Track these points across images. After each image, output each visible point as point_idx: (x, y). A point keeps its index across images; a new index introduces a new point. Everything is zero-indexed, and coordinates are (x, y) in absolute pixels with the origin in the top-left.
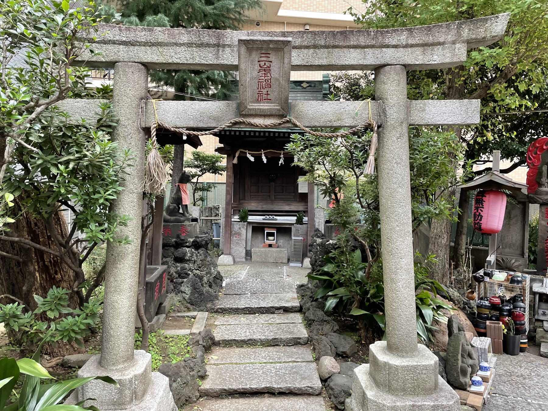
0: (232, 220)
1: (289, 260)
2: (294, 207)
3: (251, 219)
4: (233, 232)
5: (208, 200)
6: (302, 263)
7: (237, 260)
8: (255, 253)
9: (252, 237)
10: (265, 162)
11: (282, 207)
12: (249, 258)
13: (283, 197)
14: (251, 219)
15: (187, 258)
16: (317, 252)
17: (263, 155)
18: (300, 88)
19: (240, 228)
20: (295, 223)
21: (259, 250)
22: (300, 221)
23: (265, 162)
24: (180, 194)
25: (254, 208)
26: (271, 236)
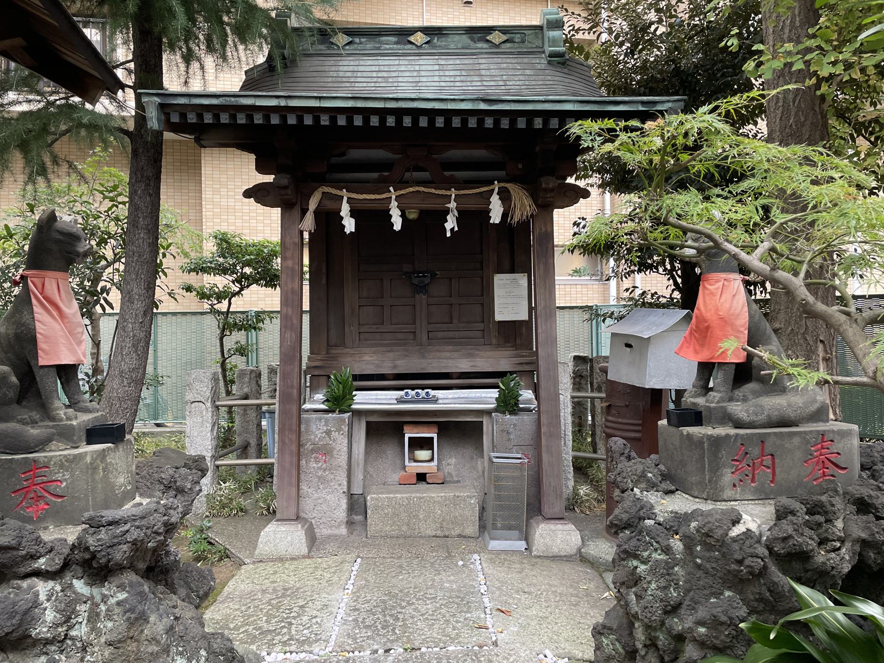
0: (307, 406)
1: (482, 528)
2: (485, 361)
3: (364, 400)
4: (309, 446)
5: (261, 353)
6: (527, 538)
7: (322, 531)
8: (376, 508)
9: (367, 453)
10: (397, 227)
12: (359, 518)
13: (451, 334)
15: (41, 631)
16: (669, 567)
17: (394, 204)
18: (485, 45)
19: (328, 433)
20: (496, 410)
21: (388, 498)
22: (509, 404)
23: (397, 227)
24: (26, 317)
25: (370, 370)
26: (422, 448)
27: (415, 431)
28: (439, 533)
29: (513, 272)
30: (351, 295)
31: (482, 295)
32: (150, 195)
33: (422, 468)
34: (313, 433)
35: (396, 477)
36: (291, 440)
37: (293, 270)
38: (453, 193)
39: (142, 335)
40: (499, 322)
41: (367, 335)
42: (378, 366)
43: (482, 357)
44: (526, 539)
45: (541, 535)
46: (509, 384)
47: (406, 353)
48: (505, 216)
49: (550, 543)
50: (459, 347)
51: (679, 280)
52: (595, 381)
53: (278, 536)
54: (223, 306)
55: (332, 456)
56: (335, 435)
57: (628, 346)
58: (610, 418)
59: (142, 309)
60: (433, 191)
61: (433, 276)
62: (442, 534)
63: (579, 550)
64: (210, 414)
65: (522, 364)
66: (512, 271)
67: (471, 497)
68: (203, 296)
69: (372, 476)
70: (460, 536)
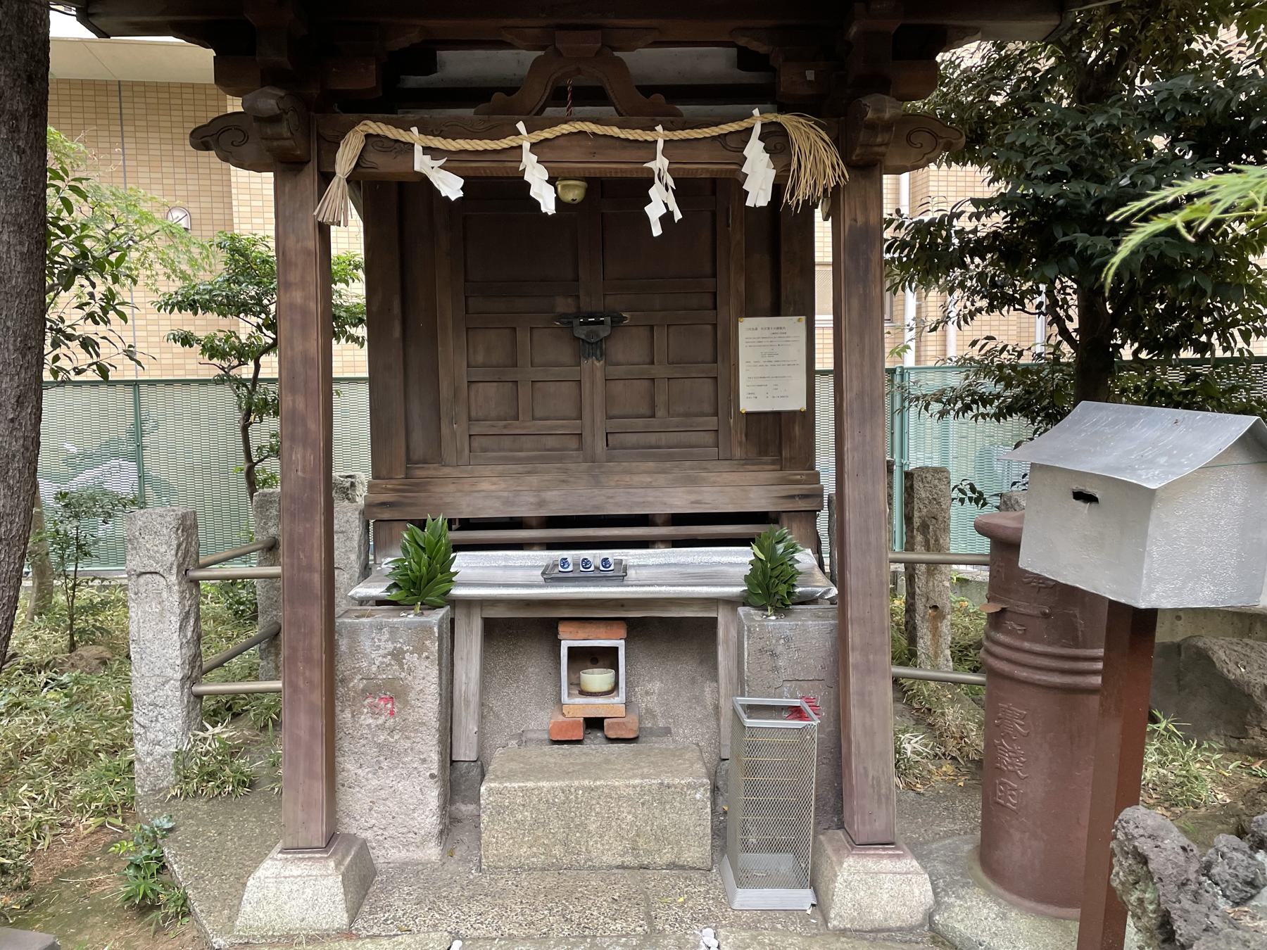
3: (482, 574)
4: (357, 683)
6: (813, 880)
7: (387, 855)
8: (499, 810)
11: (651, 495)
13: (652, 438)
14: (482, 574)
19: (397, 655)
20: (743, 600)
27: (581, 634)
28: (628, 860)
29: (779, 315)
30: (453, 361)
31: (715, 361)
32: (21, 152)
33: (596, 707)
34: (365, 655)
35: (542, 720)
36: (311, 682)
37: (304, 312)
38: (660, 135)
39: (16, 446)
40: (747, 414)
41: (484, 441)
42: (507, 502)
43: (714, 484)
44: (814, 885)
45: (848, 884)
46: (774, 549)
47: (563, 477)
48: (778, 189)
49: (867, 901)
50: (668, 464)
51: (1072, 326)
52: (916, 514)
53: (286, 887)
54: (247, 372)
55: (406, 703)
56: (411, 659)
57: (1080, 496)
58: (1001, 637)
59: (13, 393)
60: (615, 131)
61: (617, 321)
62: (635, 863)
63: (929, 916)
64: (176, 597)
65: (793, 497)
66: (776, 311)
67: (694, 787)
68: (212, 350)
69: (497, 716)
70: (672, 866)
